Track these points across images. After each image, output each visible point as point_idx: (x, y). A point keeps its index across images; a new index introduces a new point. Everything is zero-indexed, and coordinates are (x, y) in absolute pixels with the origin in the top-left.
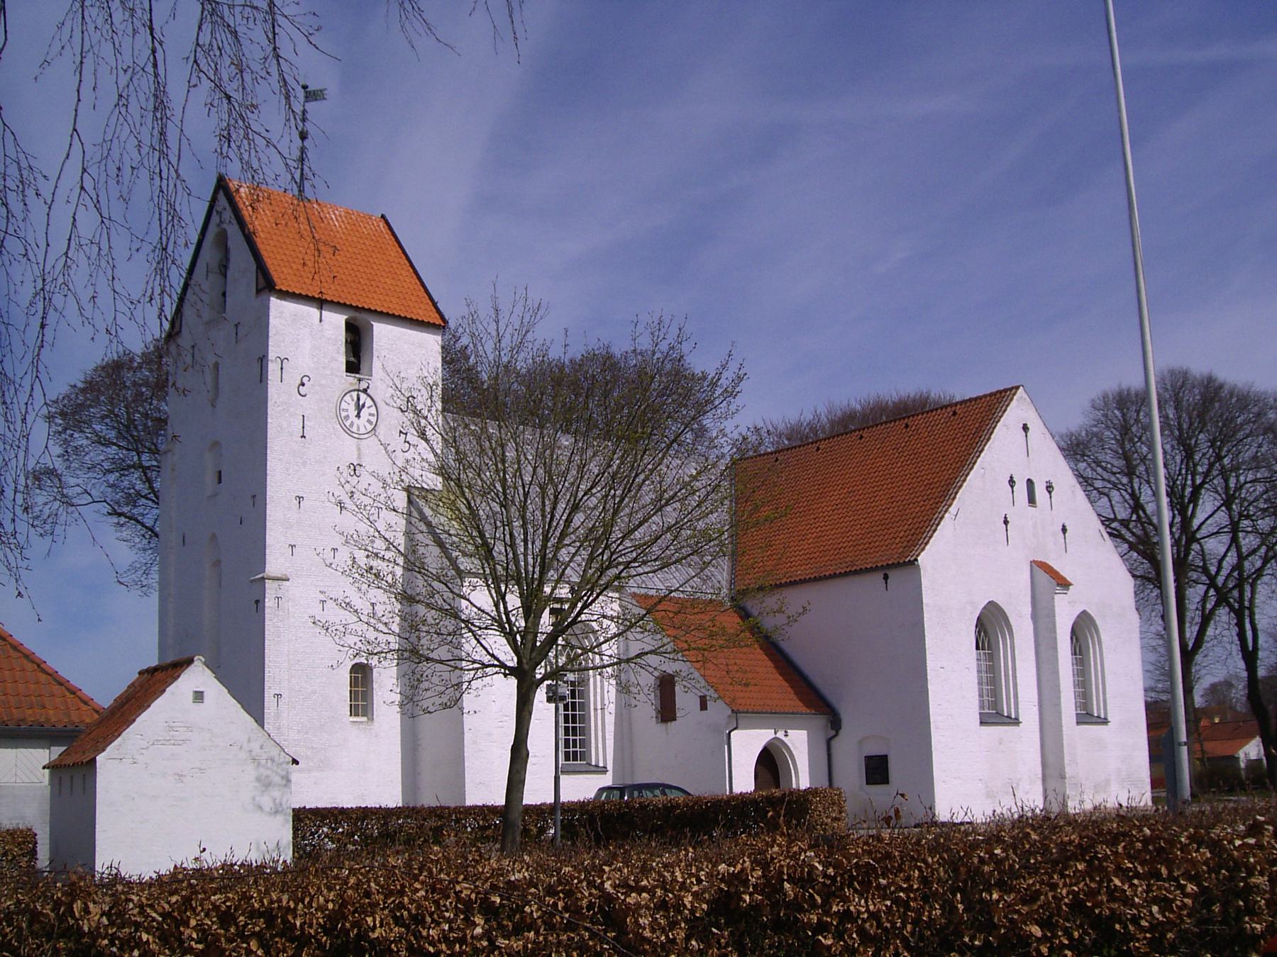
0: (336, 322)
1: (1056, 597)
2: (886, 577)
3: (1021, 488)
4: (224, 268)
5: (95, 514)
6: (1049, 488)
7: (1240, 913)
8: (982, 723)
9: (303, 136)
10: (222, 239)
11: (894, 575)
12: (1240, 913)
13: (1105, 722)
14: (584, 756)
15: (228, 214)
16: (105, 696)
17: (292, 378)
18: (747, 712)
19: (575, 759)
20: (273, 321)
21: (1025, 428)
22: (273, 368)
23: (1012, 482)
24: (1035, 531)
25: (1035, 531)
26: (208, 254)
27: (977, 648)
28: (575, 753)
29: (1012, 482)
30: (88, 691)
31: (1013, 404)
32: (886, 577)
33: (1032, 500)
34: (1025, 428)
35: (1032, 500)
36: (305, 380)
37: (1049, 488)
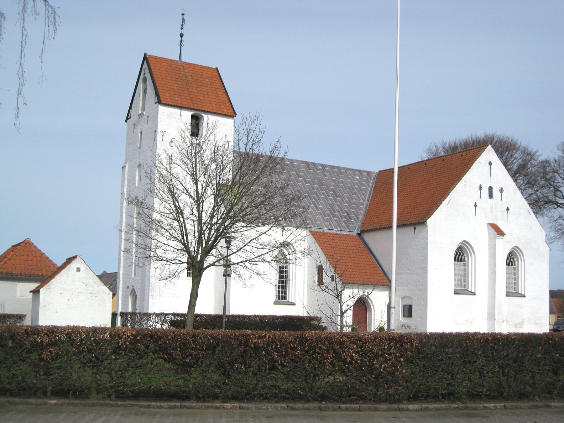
0: (187, 115)
1: (497, 240)
2: (415, 228)
3: (485, 191)
4: (145, 91)
5: (552, 161)
6: (501, 191)
7: (192, 357)
8: (455, 293)
9: (182, 35)
10: (145, 80)
11: (418, 228)
12: (192, 357)
13: (524, 296)
14: (285, 298)
15: (147, 71)
16: (59, 264)
17: (168, 139)
18: (349, 283)
19: (282, 299)
20: (160, 116)
21: (490, 163)
22: (159, 135)
23: (480, 188)
24: (491, 210)
25: (491, 210)
26: (141, 86)
27: (455, 260)
28: (282, 297)
29: (480, 188)
30: (54, 261)
31: (485, 153)
32: (415, 228)
33: (491, 196)
34: (490, 163)
35: (491, 196)
36: (173, 140)
37: (501, 191)
